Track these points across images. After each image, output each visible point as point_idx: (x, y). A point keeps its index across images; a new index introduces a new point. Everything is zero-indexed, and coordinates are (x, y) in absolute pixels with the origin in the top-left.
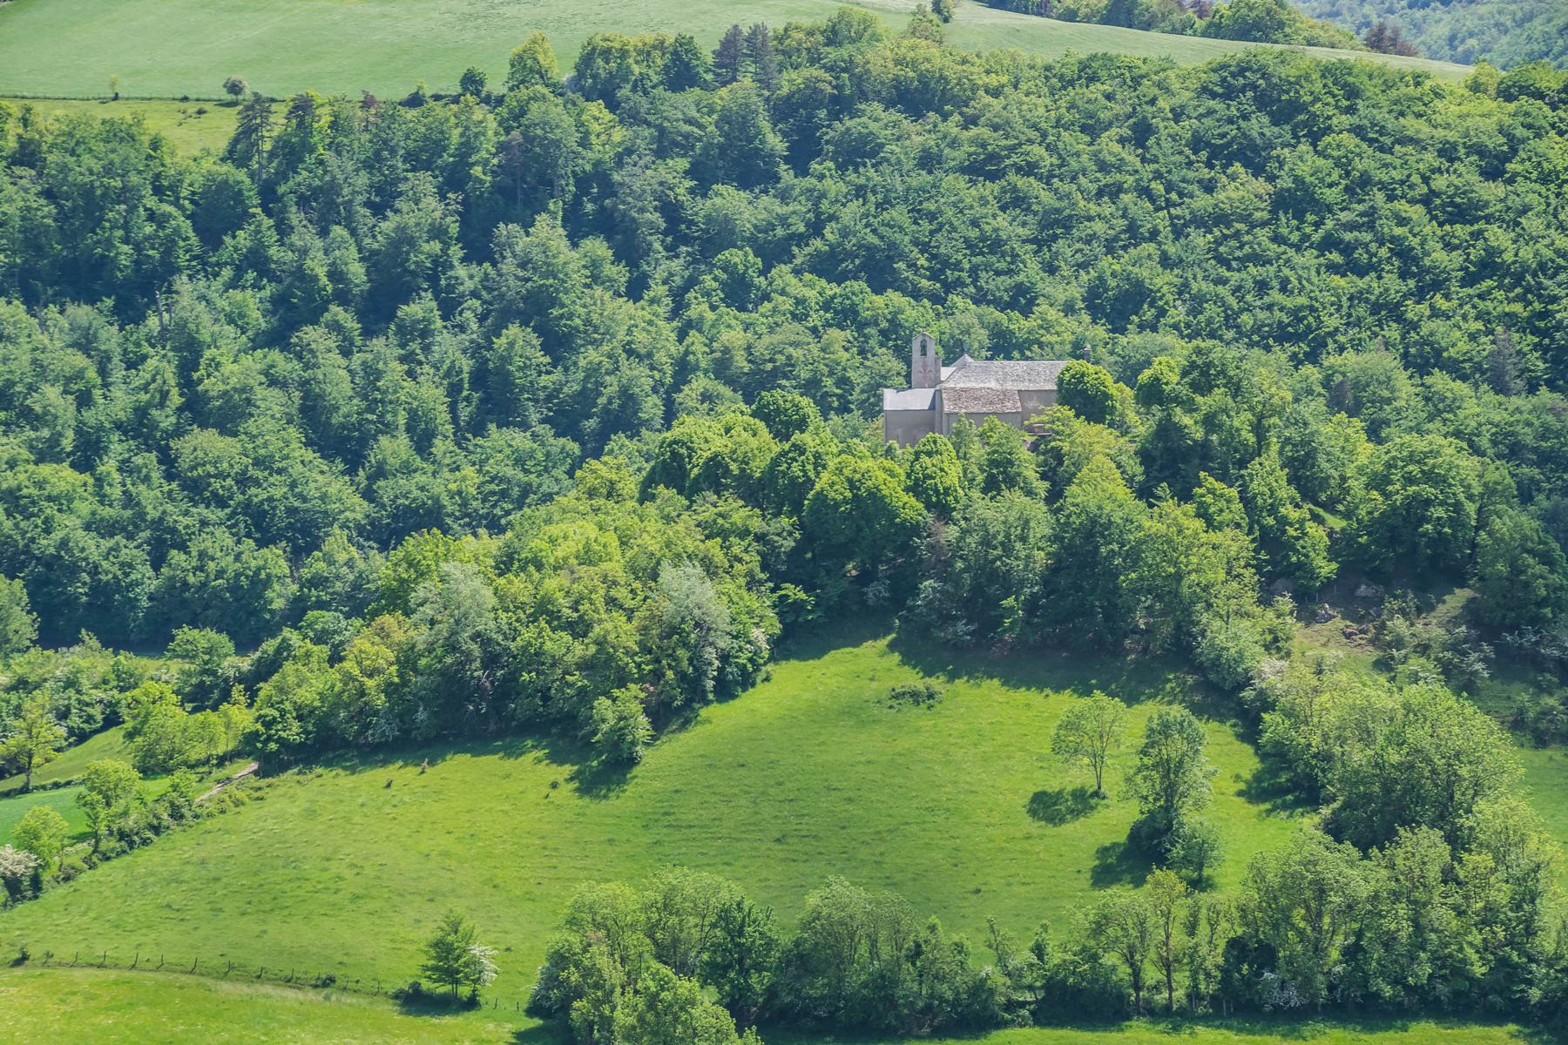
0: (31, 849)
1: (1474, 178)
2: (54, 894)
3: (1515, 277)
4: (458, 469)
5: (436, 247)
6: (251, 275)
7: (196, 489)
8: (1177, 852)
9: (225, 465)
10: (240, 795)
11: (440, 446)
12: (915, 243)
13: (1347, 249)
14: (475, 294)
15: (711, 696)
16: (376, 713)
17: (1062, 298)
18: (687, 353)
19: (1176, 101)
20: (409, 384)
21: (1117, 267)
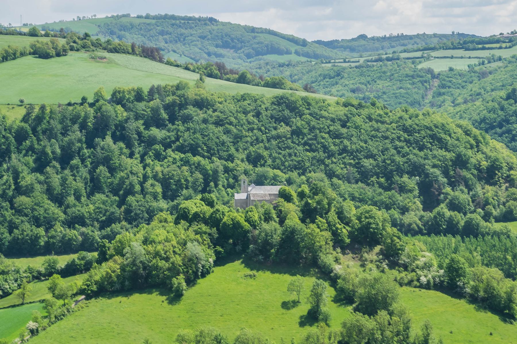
0: (36, 322)
1: (340, 127)
2: (42, 334)
3: (351, 153)
4: (88, 205)
5: (79, 145)
6: (30, 152)
7: (19, 212)
8: (321, 317)
9: (27, 206)
10: (83, 306)
11: (83, 199)
12: (203, 143)
13: (310, 145)
14: (89, 157)
15: (200, 277)
16: (115, 283)
17: (241, 158)
18: (146, 173)
19: (266, 106)
20: (74, 182)
21: (254, 150)
